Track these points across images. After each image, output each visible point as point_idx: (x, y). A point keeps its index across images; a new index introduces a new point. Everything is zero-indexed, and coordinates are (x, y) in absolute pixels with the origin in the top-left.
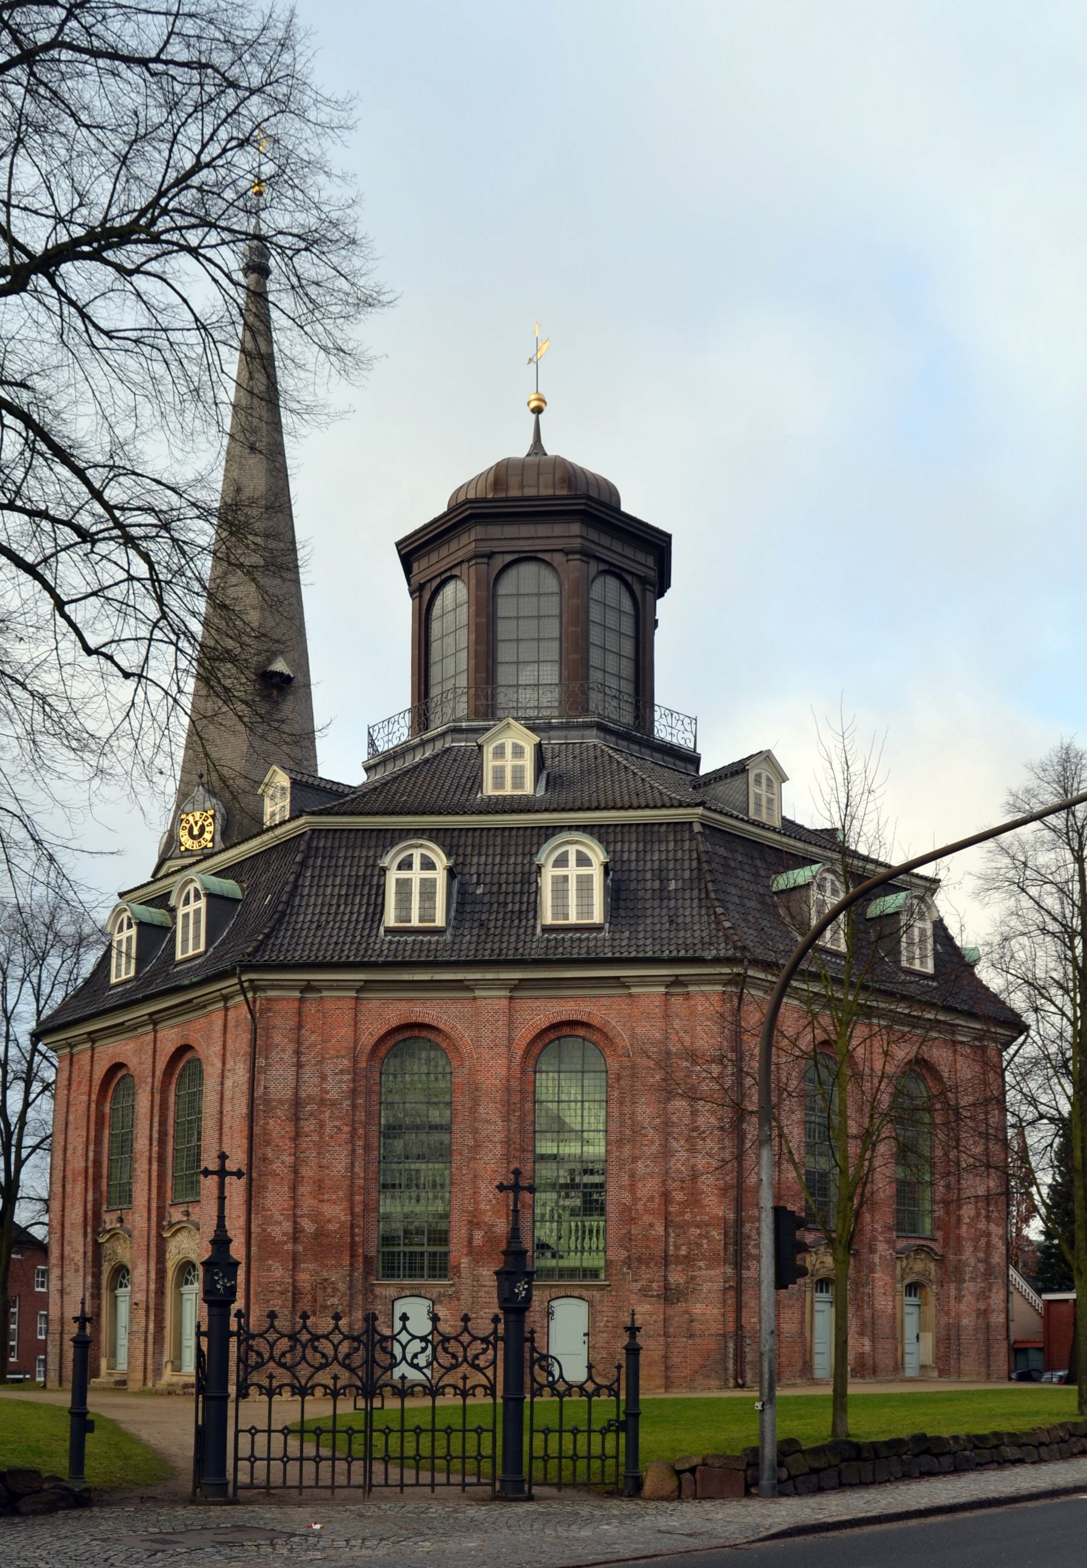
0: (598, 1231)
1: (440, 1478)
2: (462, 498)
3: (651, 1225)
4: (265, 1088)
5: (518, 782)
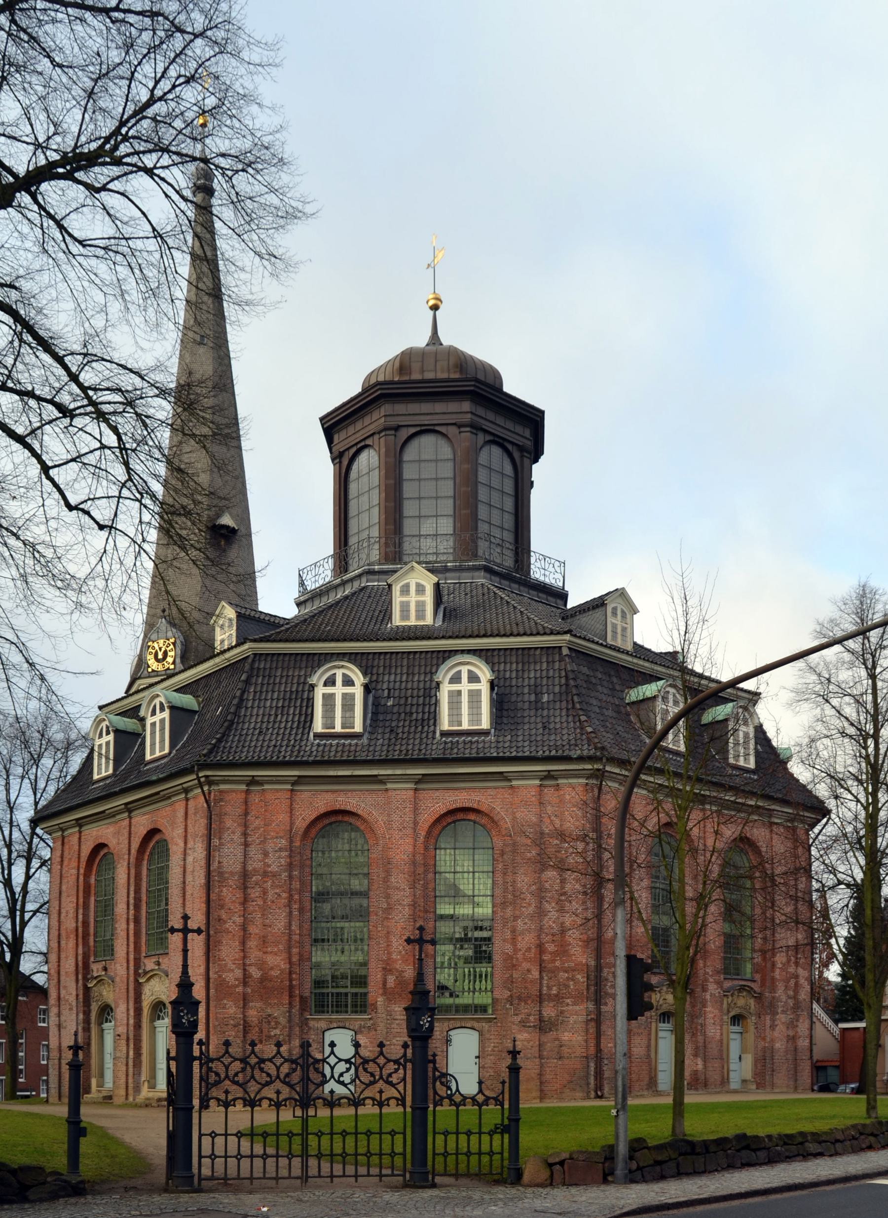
0: (486, 976)
1: (362, 1170)
2: (373, 381)
3: (529, 971)
4: (219, 862)
5: (420, 614)
